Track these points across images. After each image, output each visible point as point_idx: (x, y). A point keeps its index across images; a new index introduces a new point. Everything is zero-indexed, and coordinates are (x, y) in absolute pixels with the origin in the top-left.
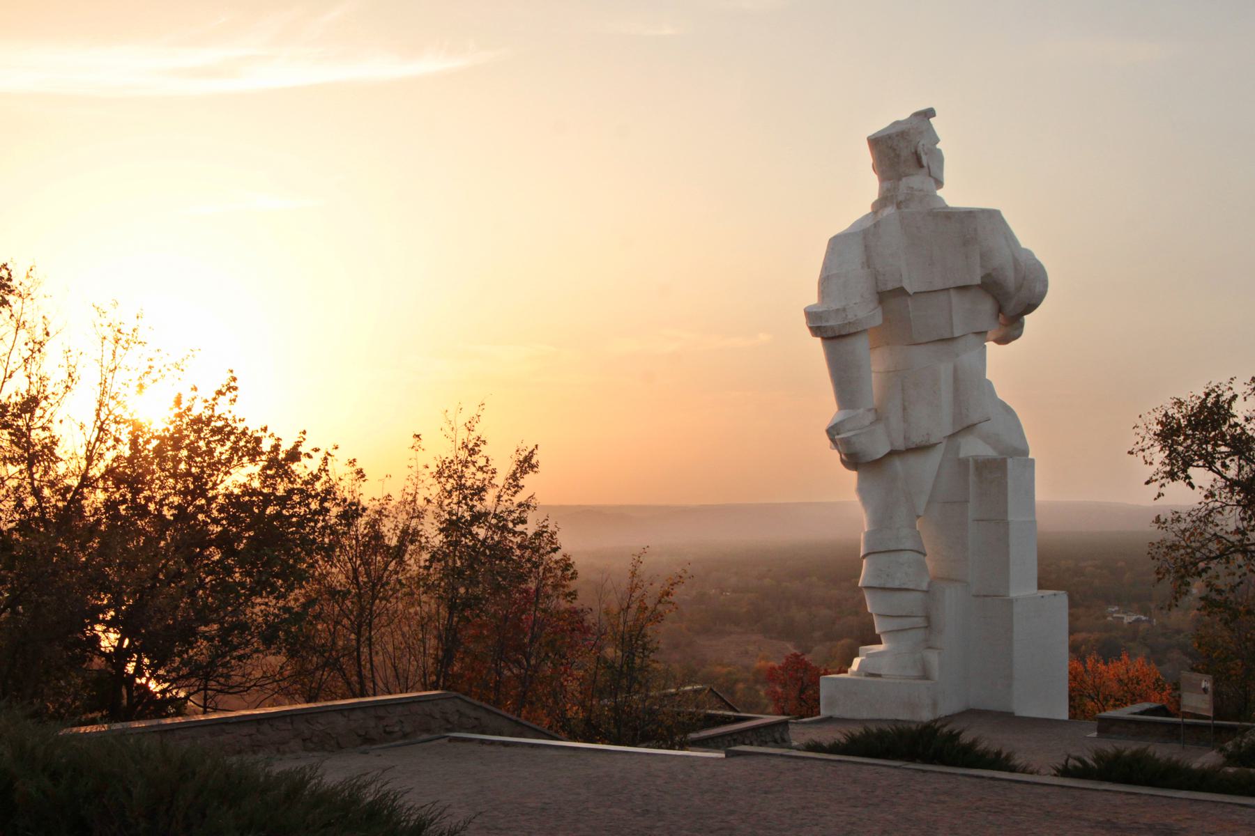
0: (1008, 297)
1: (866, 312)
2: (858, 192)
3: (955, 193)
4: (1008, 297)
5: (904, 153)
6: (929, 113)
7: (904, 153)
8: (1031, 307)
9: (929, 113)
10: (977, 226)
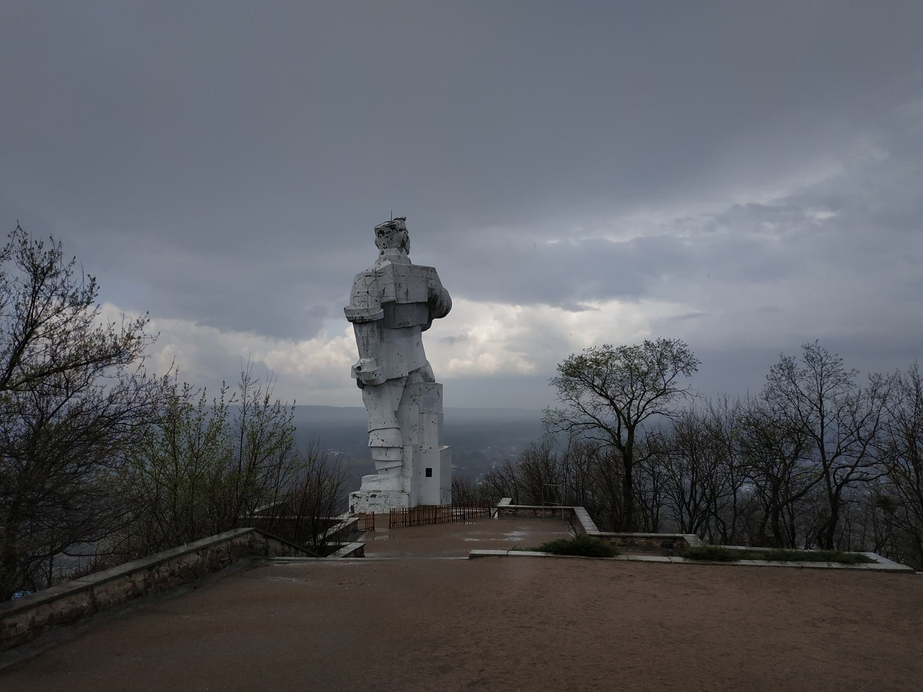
1: (379, 313)
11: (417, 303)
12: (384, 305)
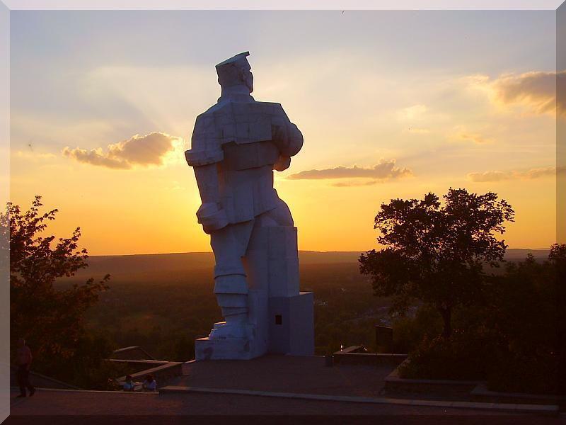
0: (281, 140)
1: (217, 155)
2: (209, 93)
3: (261, 93)
4: (281, 140)
5: (235, 74)
6: (247, 54)
7: (235, 74)
8: (296, 150)
9: (247, 54)
10: (274, 111)
11: (260, 142)
12: (224, 147)
